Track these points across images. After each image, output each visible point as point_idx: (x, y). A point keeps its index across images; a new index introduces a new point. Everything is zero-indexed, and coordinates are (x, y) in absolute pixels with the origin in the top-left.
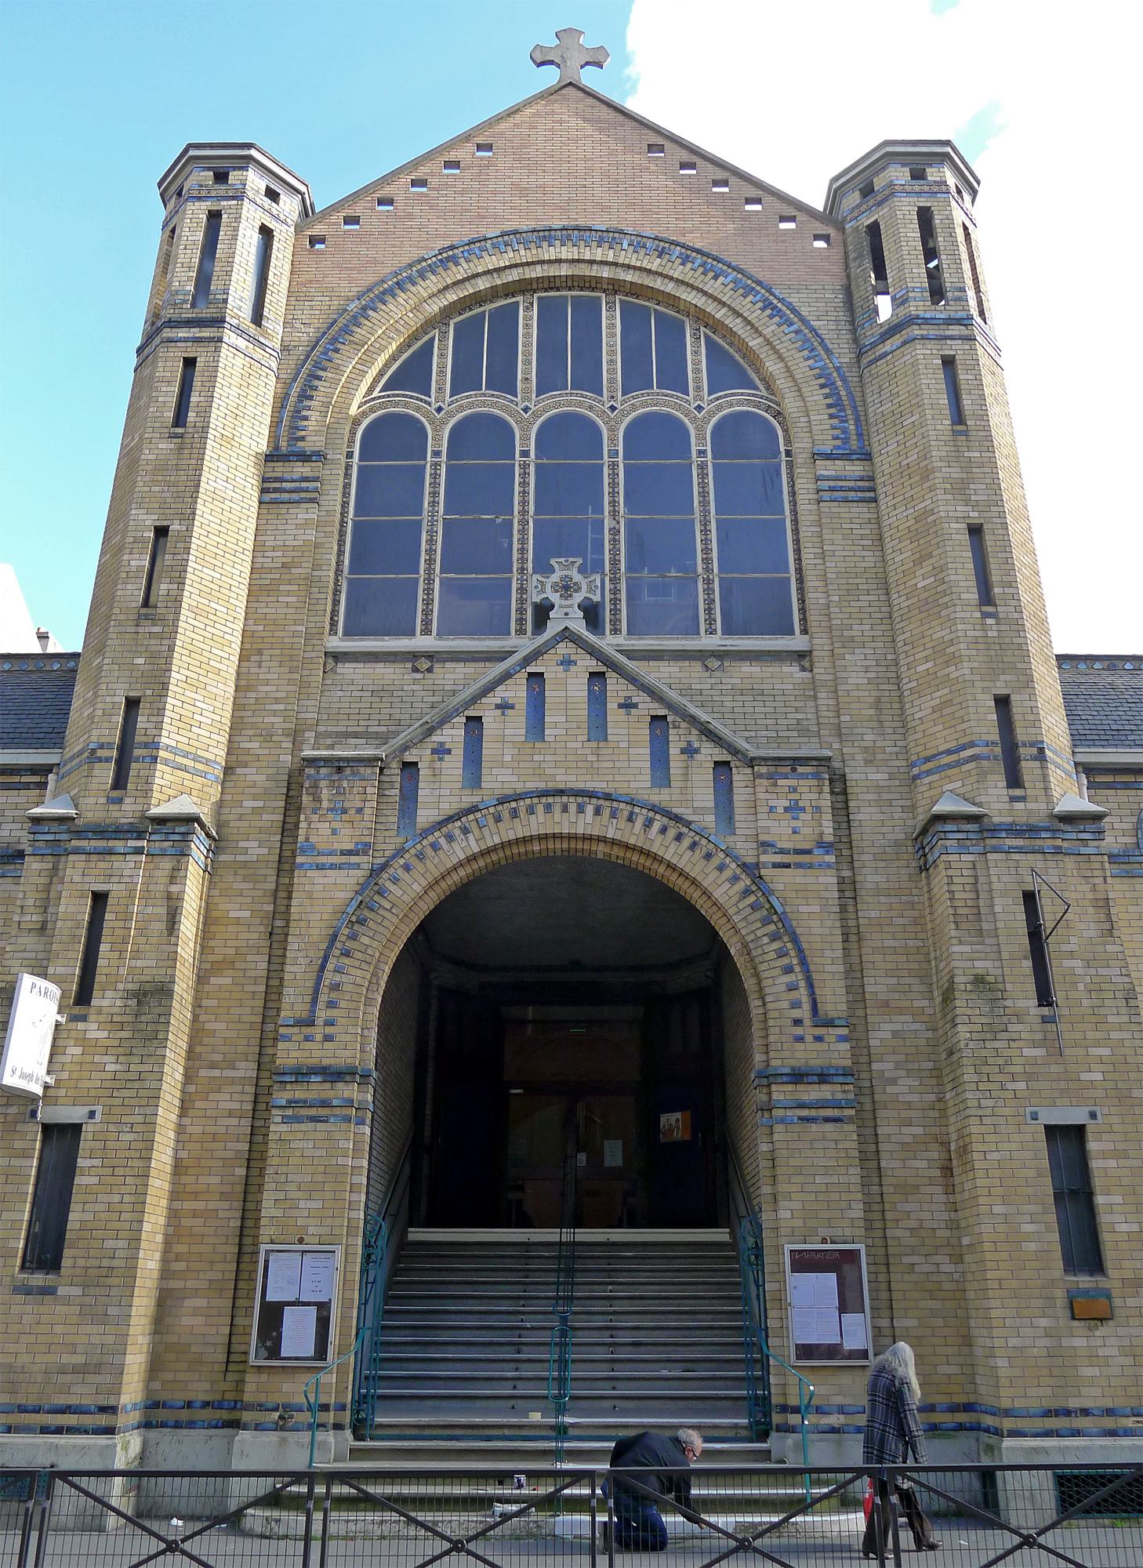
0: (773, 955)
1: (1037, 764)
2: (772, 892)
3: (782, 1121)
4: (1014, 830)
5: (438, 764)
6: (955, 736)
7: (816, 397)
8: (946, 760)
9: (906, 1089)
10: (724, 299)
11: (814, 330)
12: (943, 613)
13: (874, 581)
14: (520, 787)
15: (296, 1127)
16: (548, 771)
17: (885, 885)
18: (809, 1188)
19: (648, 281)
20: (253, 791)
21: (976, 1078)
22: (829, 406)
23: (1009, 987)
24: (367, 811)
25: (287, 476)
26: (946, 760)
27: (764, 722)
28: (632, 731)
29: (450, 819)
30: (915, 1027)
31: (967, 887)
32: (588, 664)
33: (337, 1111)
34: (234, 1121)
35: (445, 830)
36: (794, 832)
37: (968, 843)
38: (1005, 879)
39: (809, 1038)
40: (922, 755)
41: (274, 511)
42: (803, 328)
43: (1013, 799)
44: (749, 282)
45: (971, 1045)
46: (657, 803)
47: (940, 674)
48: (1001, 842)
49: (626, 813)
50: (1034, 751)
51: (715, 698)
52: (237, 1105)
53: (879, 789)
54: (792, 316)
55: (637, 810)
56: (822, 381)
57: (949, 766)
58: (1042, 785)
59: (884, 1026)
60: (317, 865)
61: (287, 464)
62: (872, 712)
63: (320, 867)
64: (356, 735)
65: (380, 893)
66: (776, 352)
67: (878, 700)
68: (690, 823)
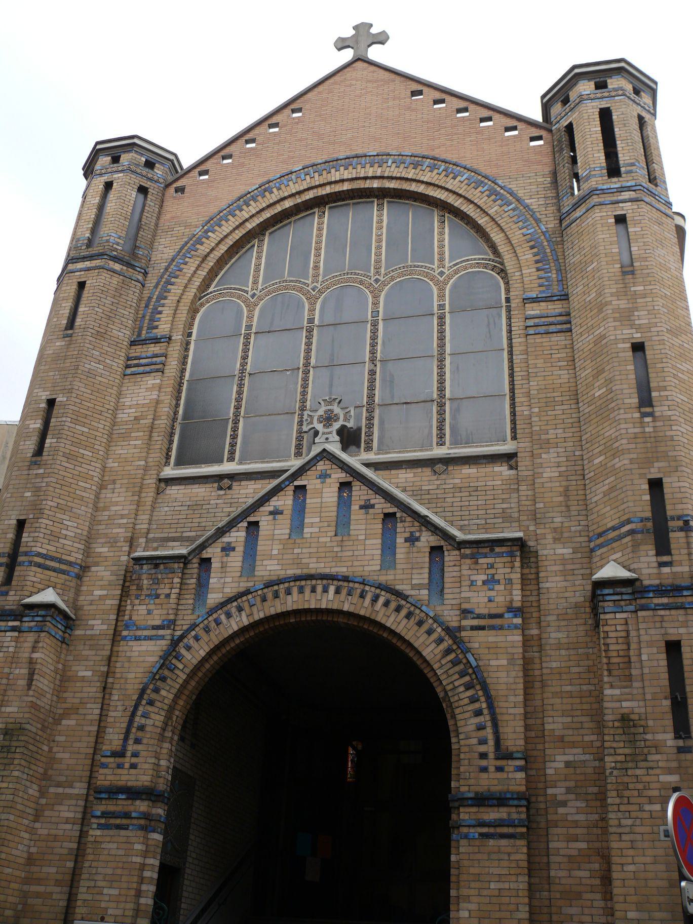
0: (466, 701)
1: (682, 534)
2: (469, 650)
3: (466, 837)
4: (661, 591)
5: (225, 559)
6: (618, 515)
7: (527, 256)
8: (612, 535)
9: (573, 811)
10: (460, 192)
11: (528, 206)
12: (612, 416)
13: (568, 393)
14: (282, 574)
15: (106, 832)
16: (304, 561)
17: (565, 641)
18: (485, 892)
19: (406, 186)
20: (101, 583)
21: (617, 801)
22: (537, 262)
23: (650, 723)
24: (173, 596)
25: (144, 355)
26: (612, 535)
27: (476, 512)
28: (368, 527)
29: (230, 600)
30: (583, 758)
31: (620, 640)
32: (339, 475)
33: (135, 822)
34: (69, 826)
35: (225, 609)
36: (490, 601)
37: (623, 603)
38: (652, 632)
39: (492, 769)
40: (597, 531)
41: (133, 380)
42: (519, 205)
43: (661, 565)
44: (480, 177)
45: (615, 772)
46: (384, 583)
47: (609, 465)
48: (649, 601)
49: (359, 591)
50: (680, 523)
51: (439, 496)
52: (71, 815)
53: (564, 561)
54: (511, 198)
55: (367, 588)
56: (532, 243)
57: (614, 540)
58: (686, 551)
59: (558, 758)
60: (136, 637)
61: (144, 346)
62: (561, 499)
63: (138, 639)
64: (174, 539)
65: (176, 658)
66: (499, 225)
67: (567, 489)
68: (408, 597)
